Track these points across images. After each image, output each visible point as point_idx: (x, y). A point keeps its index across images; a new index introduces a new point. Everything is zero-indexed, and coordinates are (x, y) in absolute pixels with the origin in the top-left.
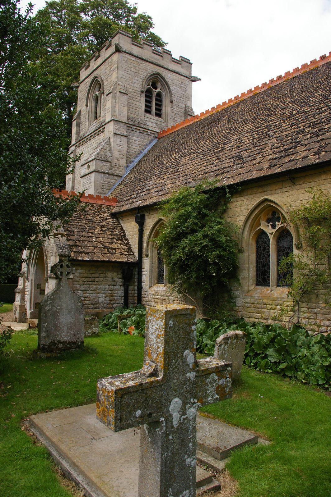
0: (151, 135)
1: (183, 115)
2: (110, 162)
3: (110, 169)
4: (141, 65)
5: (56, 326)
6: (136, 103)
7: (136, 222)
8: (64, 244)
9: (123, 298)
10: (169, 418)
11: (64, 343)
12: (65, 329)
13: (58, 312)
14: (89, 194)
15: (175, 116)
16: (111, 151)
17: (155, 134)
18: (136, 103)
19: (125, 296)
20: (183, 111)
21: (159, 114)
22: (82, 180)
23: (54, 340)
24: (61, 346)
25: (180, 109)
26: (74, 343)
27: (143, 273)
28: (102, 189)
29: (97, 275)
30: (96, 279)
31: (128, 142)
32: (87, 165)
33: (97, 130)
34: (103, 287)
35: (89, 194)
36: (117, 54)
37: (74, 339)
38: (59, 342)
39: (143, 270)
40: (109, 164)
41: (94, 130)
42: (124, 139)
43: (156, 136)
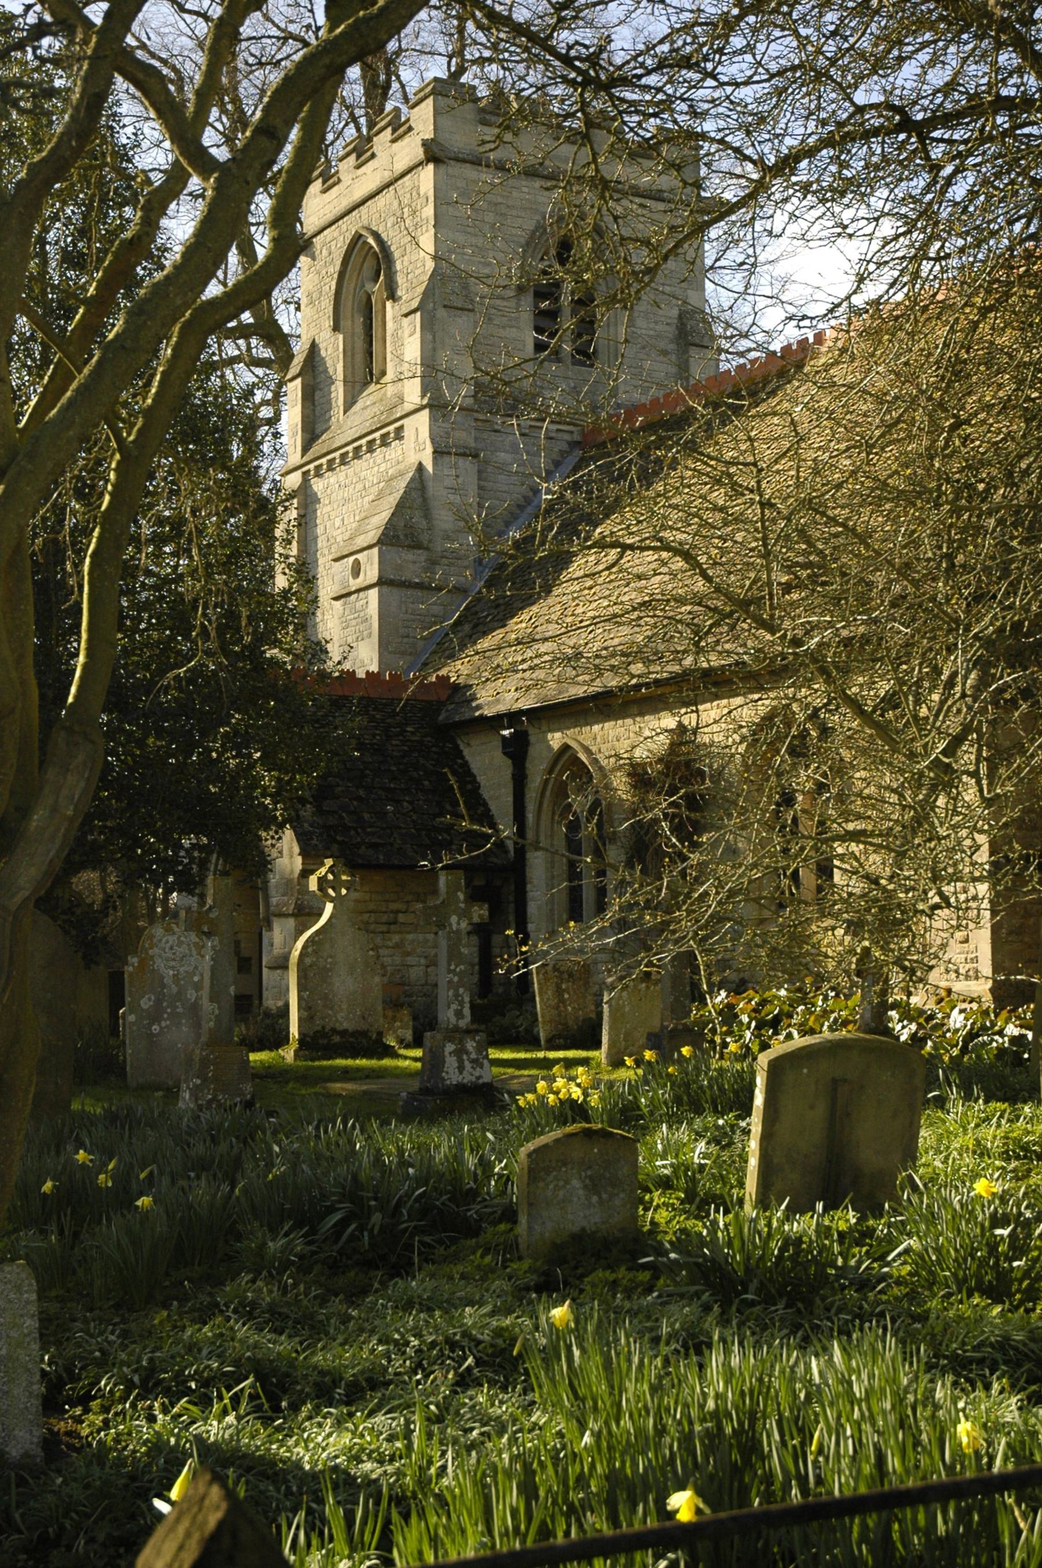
0: (560, 435)
1: (672, 347)
2: (427, 549)
3: (426, 570)
4: (515, 194)
5: (325, 997)
6: (502, 333)
7: (505, 754)
8: (311, 826)
9: (477, 968)
10: (450, 925)
11: (344, 1033)
12: (344, 1006)
13: (330, 970)
14: (367, 672)
15: (642, 356)
16: (427, 514)
17: (572, 432)
18: (502, 333)
19: (480, 964)
20: (671, 331)
21: (585, 355)
22: (338, 604)
23: (323, 1027)
24: (337, 1039)
25: (659, 327)
26: (364, 1034)
27: (530, 895)
28: (405, 640)
29: (402, 906)
30: (401, 918)
31: (479, 472)
32: (352, 559)
33: (377, 430)
34: (421, 937)
35: (367, 672)
36: (431, 167)
37: (362, 1026)
38: (334, 1031)
39: (529, 887)
40: (421, 556)
41: (367, 427)
42: (467, 465)
43: (577, 437)
